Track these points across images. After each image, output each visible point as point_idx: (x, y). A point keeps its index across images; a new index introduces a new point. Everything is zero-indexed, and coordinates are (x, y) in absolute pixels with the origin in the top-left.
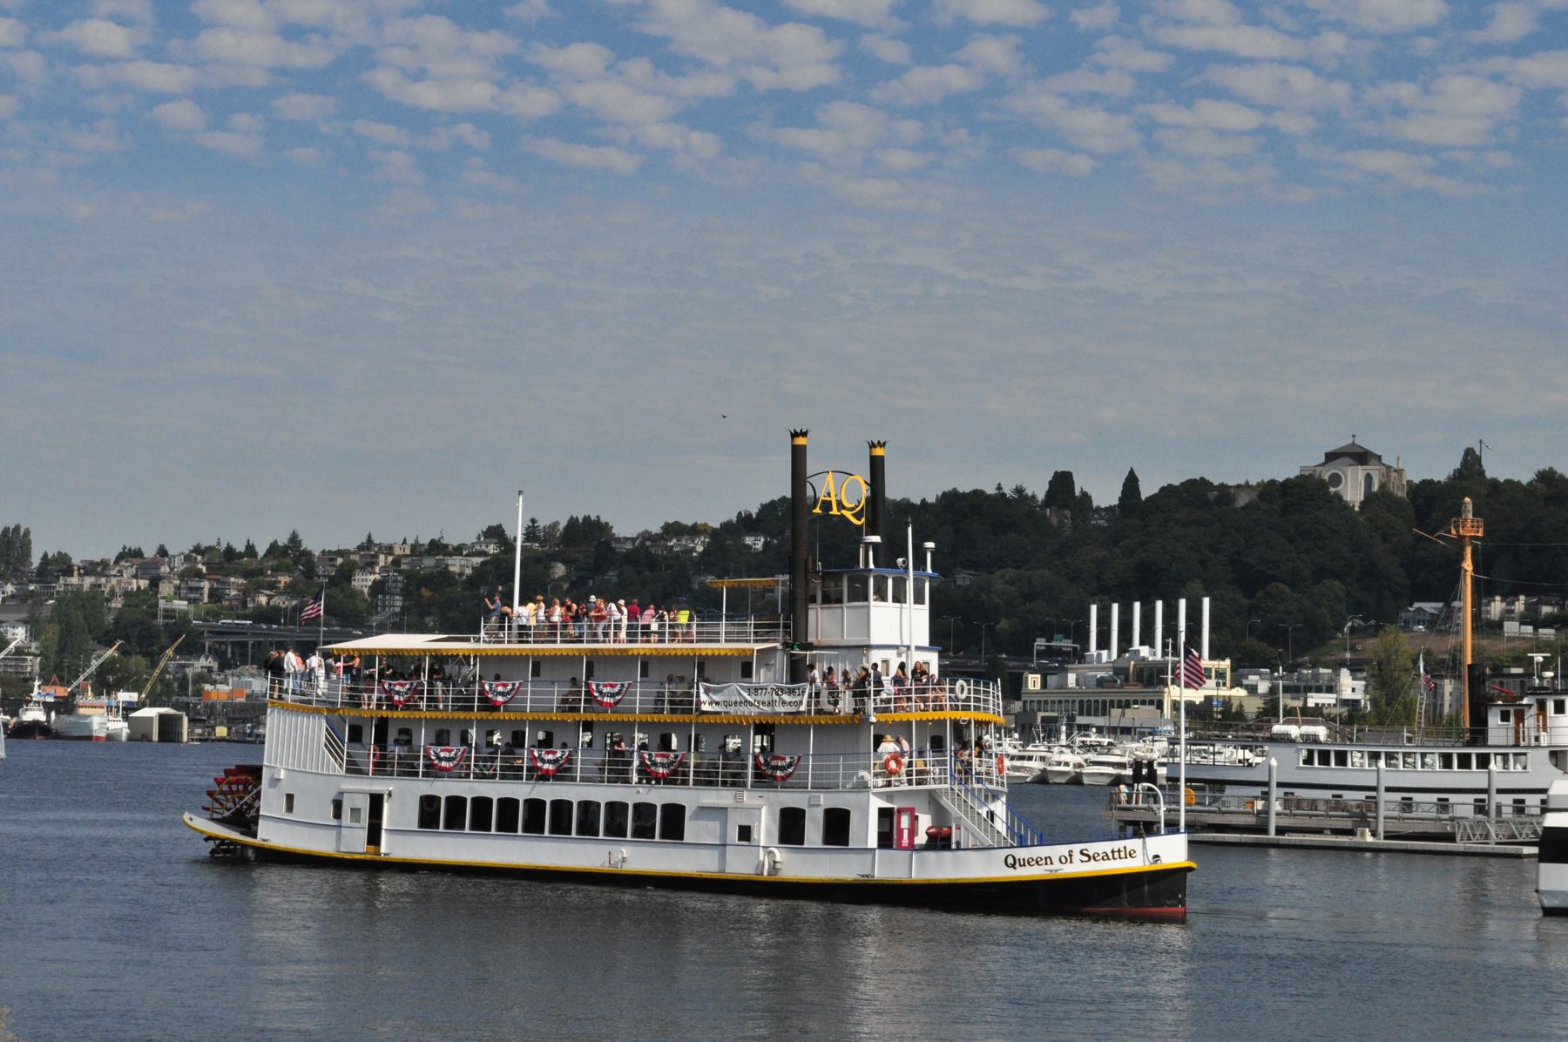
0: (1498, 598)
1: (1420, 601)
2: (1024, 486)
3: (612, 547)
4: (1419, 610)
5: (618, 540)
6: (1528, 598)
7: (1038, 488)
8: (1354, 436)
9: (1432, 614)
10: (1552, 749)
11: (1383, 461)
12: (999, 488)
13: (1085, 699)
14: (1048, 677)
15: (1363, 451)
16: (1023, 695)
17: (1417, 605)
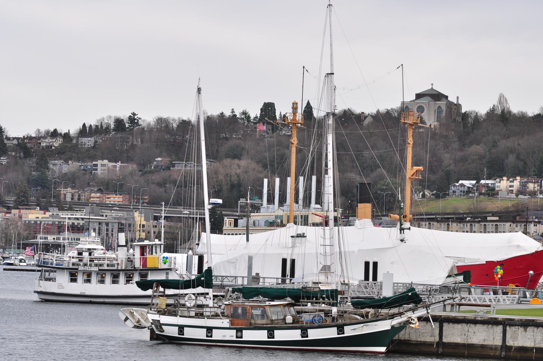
0: (505, 178)
1: (462, 180)
2: (247, 111)
3: (5, 143)
4: (462, 185)
5: (8, 139)
7: (255, 112)
8: (432, 84)
9: (469, 187)
10: (196, 312)
15: (438, 93)
16: (224, 231)
17: (461, 182)
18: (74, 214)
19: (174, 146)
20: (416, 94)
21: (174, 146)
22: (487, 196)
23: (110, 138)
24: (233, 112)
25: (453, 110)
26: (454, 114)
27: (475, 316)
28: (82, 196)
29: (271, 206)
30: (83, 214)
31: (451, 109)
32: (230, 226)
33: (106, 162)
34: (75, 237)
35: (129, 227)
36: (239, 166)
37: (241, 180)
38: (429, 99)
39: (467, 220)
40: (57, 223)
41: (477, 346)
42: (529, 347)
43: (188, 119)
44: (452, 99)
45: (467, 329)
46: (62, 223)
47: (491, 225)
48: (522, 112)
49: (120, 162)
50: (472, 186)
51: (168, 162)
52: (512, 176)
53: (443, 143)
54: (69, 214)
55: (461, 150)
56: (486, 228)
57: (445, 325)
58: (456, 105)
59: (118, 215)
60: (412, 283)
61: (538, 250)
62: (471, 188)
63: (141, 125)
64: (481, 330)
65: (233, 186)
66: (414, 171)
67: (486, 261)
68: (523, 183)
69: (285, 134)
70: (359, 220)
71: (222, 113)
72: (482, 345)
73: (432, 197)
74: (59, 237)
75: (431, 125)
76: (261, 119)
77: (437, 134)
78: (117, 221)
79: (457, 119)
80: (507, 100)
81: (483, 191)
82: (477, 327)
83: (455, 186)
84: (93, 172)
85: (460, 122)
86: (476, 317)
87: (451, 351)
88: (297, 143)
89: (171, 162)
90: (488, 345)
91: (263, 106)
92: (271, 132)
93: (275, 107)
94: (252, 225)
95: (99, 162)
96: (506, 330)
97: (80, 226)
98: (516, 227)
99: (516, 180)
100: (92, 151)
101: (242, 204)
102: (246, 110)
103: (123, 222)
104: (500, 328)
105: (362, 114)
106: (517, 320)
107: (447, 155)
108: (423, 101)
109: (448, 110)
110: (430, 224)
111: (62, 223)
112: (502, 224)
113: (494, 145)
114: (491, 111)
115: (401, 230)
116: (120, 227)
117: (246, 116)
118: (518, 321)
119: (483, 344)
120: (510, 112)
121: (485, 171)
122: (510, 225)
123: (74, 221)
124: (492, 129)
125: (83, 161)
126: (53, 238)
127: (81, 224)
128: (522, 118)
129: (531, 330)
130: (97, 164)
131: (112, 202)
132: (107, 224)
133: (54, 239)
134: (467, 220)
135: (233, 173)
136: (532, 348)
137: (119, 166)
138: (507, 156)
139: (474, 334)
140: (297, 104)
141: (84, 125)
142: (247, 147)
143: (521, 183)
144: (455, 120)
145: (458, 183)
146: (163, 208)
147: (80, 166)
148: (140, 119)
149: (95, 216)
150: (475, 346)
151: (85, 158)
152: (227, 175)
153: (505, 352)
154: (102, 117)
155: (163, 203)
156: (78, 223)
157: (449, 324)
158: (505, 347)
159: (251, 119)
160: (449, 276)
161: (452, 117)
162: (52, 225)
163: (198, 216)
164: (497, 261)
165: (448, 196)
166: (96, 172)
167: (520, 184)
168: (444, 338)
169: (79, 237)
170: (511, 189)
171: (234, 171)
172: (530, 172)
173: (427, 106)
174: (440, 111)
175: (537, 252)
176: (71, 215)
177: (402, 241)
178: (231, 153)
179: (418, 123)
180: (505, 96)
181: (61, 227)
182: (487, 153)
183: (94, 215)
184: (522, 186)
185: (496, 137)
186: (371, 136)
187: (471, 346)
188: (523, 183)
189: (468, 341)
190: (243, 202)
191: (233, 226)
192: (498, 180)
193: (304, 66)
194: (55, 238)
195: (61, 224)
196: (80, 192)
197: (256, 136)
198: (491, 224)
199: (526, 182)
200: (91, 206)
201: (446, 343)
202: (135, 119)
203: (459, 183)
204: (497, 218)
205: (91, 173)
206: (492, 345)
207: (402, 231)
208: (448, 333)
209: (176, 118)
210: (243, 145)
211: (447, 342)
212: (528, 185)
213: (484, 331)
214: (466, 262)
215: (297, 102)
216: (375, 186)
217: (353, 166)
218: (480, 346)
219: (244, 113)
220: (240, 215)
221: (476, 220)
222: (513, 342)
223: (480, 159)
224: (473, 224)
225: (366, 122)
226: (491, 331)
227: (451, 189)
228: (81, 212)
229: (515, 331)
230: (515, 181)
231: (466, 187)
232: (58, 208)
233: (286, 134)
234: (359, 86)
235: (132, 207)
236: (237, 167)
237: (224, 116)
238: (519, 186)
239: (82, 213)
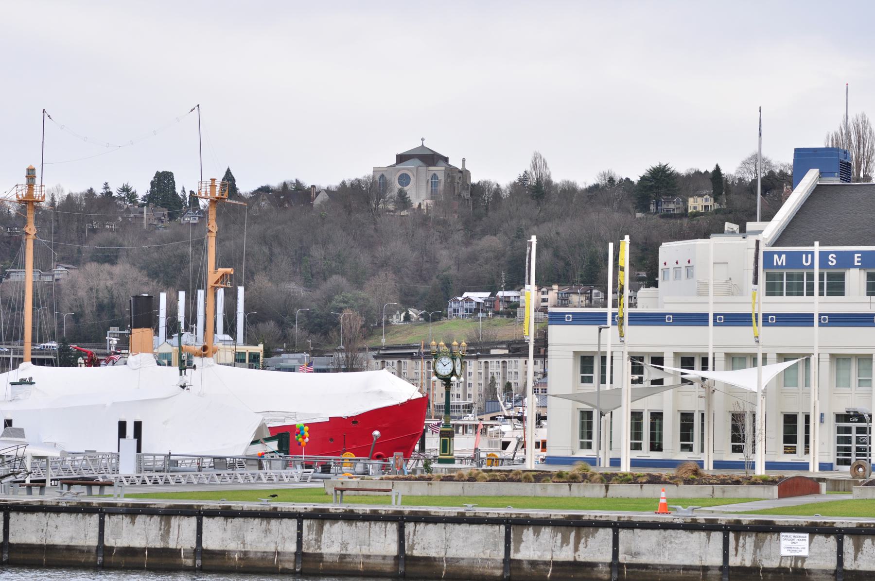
1: (469, 291)
2: (130, 185)
4: (468, 300)
6: (562, 288)
7: (142, 188)
8: (423, 139)
9: (478, 303)
11: (450, 163)
15: (432, 153)
17: (466, 295)
19: (10, 244)
20: (397, 156)
21: (10, 244)
22: (505, 317)
24: (106, 188)
25: (457, 180)
27: (58, 501)
31: (453, 178)
36: (110, 274)
37: (114, 297)
38: (417, 162)
41: (61, 549)
42: (139, 548)
44: (455, 162)
45: (46, 522)
47: (495, 362)
48: (568, 182)
50: (483, 302)
53: (440, 232)
55: (467, 244)
56: (488, 368)
57: (13, 516)
58: (460, 172)
60: (170, 453)
61: (412, 399)
64: (67, 522)
65: (101, 307)
66: (219, 275)
67: (330, 418)
68: (564, 295)
69: (188, 223)
70: (133, 355)
71: (91, 189)
72: (68, 546)
73: (420, 319)
75: (420, 204)
76: (150, 198)
77: (429, 218)
79: (462, 195)
81: (501, 309)
82: (61, 518)
83: (456, 301)
85: (468, 200)
86: (59, 502)
87: (22, 557)
88: (35, 233)
90: (77, 546)
91: (154, 178)
92: (167, 219)
93: (175, 180)
96: (104, 522)
99: (552, 290)
102: (129, 185)
104: (96, 517)
105: (312, 189)
106: (120, 505)
107: (445, 253)
108: (409, 167)
109: (449, 181)
110: (399, 362)
112: (513, 360)
113: (519, 235)
115: (181, 370)
117: (128, 194)
118: (122, 507)
119: (70, 544)
120: (549, 182)
121: (503, 276)
124: (517, 210)
128: (569, 191)
129: (141, 520)
135: (102, 286)
136: (143, 550)
139: (56, 530)
140: (33, 170)
142: (126, 243)
143: (560, 295)
144: (459, 195)
145: (461, 296)
150: (57, 549)
152: (91, 289)
153: (103, 557)
157: (18, 514)
158: (615, 565)
160: (254, 442)
161: (454, 191)
163: (12, 356)
164: (347, 417)
165: (445, 318)
167: (558, 296)
168: (10, 536)
170: (545, 304)
171: (102, 282)
172: (575, 277)
173: (415, 174)
175: (410, 401)
177: (183, 387)
178: (100, 255)
179: (224, 199)
180: (543, 156)
184: (562, 300)
185: (524, 222)
186: (323, 224)
187: (51, 549)
188: (564, 295)
189: (47, 541)
190: (114, 333)
193: (44, 110)
197: (142, 225)
198: (495, 360)
199: (567, 293)
201: (13, 544)
203: (463, 296)
204: (507, 352)
206: (83, 546)
207: (183, 371)
208: (16, 529)
210: (121, 240)
211: (15, 543)
212: (570, 298)
213: (72, 524)
214: (298, 419)
215: (34, 166)
216: (329, 304)
217: (295, 272)
218: (65, 547)
219: (126, 189)
221: (473, 355)
222: (113, 541)
223: (497, 258)
224: (468, 361)
225: (317, 201)
226: (81, 523)
227: (451, 307)
229: (117, 524)
230: (550, 292)
231: (474, 303)
233: (191, 222)
234: (131, 141)
236: (108, 277)
237: (94, 194)
238: (557, 300)
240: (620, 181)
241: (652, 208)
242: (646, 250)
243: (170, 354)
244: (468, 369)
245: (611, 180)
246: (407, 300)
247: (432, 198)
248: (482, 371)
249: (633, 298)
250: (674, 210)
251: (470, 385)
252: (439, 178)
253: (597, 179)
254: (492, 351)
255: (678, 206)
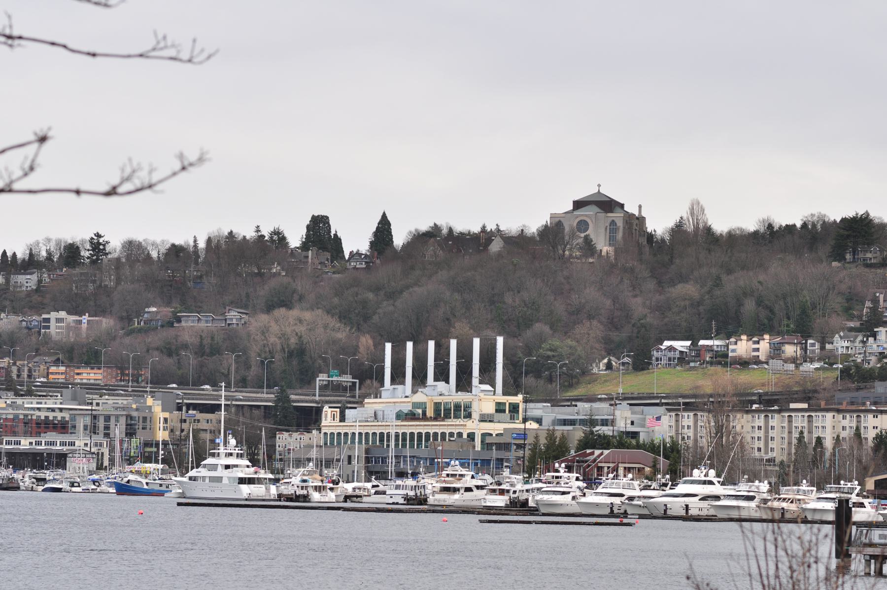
0: (744, 337)
2: (282, 229)
4: (671, 349)
8: (599, 186)
9: (681, 352)
11: (625, 209)
12: (258, 230)
13: (385, 432)
14: (347, 411)
15: (609, 200)
16: (323, 428)
17: (667, 343)
18: (43, 401)
23: (62, 275)
24: (258, 231)
25: (635, 227)
26: (636, 233)
28: (35, 372)
29: (400, 387)
30: (58, 401)
32: (334, 420)
33: (63, 314)
34: (67, 441)
35: (143, 422)
39: (754, 408)
40: (21, 417)
43: (185, 243)
44: (631, 208)
46: (30, 417)
47: (800, 416)
49: (87, 314)
51: (170, 314)
52: (755, 331)
54: (35, 401)
58: (637, 218)
59: (117, 403)
62: (685, 353)
63: (110, 253)
68: (776, 345)
71: (231, 232)
74: (40, 440)
78: (124, 413)
80: (704, 210)
83: (659, 350)
84: (43, 331)
89: (174, 313)
91: (310, 221)
93: (330, 223)
94: (372, 419)
95: (53, 315)
97: (58, 420)
98: (843, 419)
99: (764, 339)
100: (36, 298)
101: (321, 382)
103: (135, 414)
108: (587, 212)
110: (695, 415)
111: (30, 417)
112: (820, 414)
114: (677, 227)
116: (129, 422)
122: (834, 416)
123: (47, 414)
125: (24, 314)
126: (30, 443)
127: (59, 418)
128: (734, 240)
130: (49, 318)
131: (85, 381)
132: (107, 418)
133: (31, 443)
134: (754, 408)
137: (85, 321)
138: (740, 304)
141: (4, 253)
146: (223, 393)
147: (22, 321)
148: (108, 242)
149: (80, 405)
151: (24, 308)
154: (36, 239)
155: (223, 384)
156: (54, 417)
159: (266, 238)
162: (13, 420)
166: (47, 331)
169: (73, 441)
172: (780, 326)
174: (613, 228)
176: (38, 403)
178: (275, 299)
180: (702, 203)
181: (27, 423)
182: (707, 297)
183: (77, 402)
188: (776, 345)
190: (323, 380)
191: (338, 419)
192: (733, 340)
194: (87, 444)
195: (29, 419)
196: (30, 365)
198: (800, 414)
199: (780, 343)
200: (72, 388)
202: (100, 244)
204: (805, 406)
205: (39, 332)
209: (158, 240)
212: (783, 348)
220: (320, 400)
224: (770, 415)
228: (53, 398)
230: (761, 342)
231: (677, 352)
232: (13, 393)
233: (357, 267)
235: (130, 389)
237: (234, 237)
239: (55, 401)
240: (780, 228)
241: (848, 257)
242: (851, 299)
243: (425, 403)
244: (770, 422)
245: (770, 226)
246: (613, 348)
247: (610, 245)
248: (786, 424)
249: (850, 349)
250: (871, 259)
251: (772, 439)
252: (618, 225)
253: (757, 226)
254: (791, 404)
255: (875, 255)
